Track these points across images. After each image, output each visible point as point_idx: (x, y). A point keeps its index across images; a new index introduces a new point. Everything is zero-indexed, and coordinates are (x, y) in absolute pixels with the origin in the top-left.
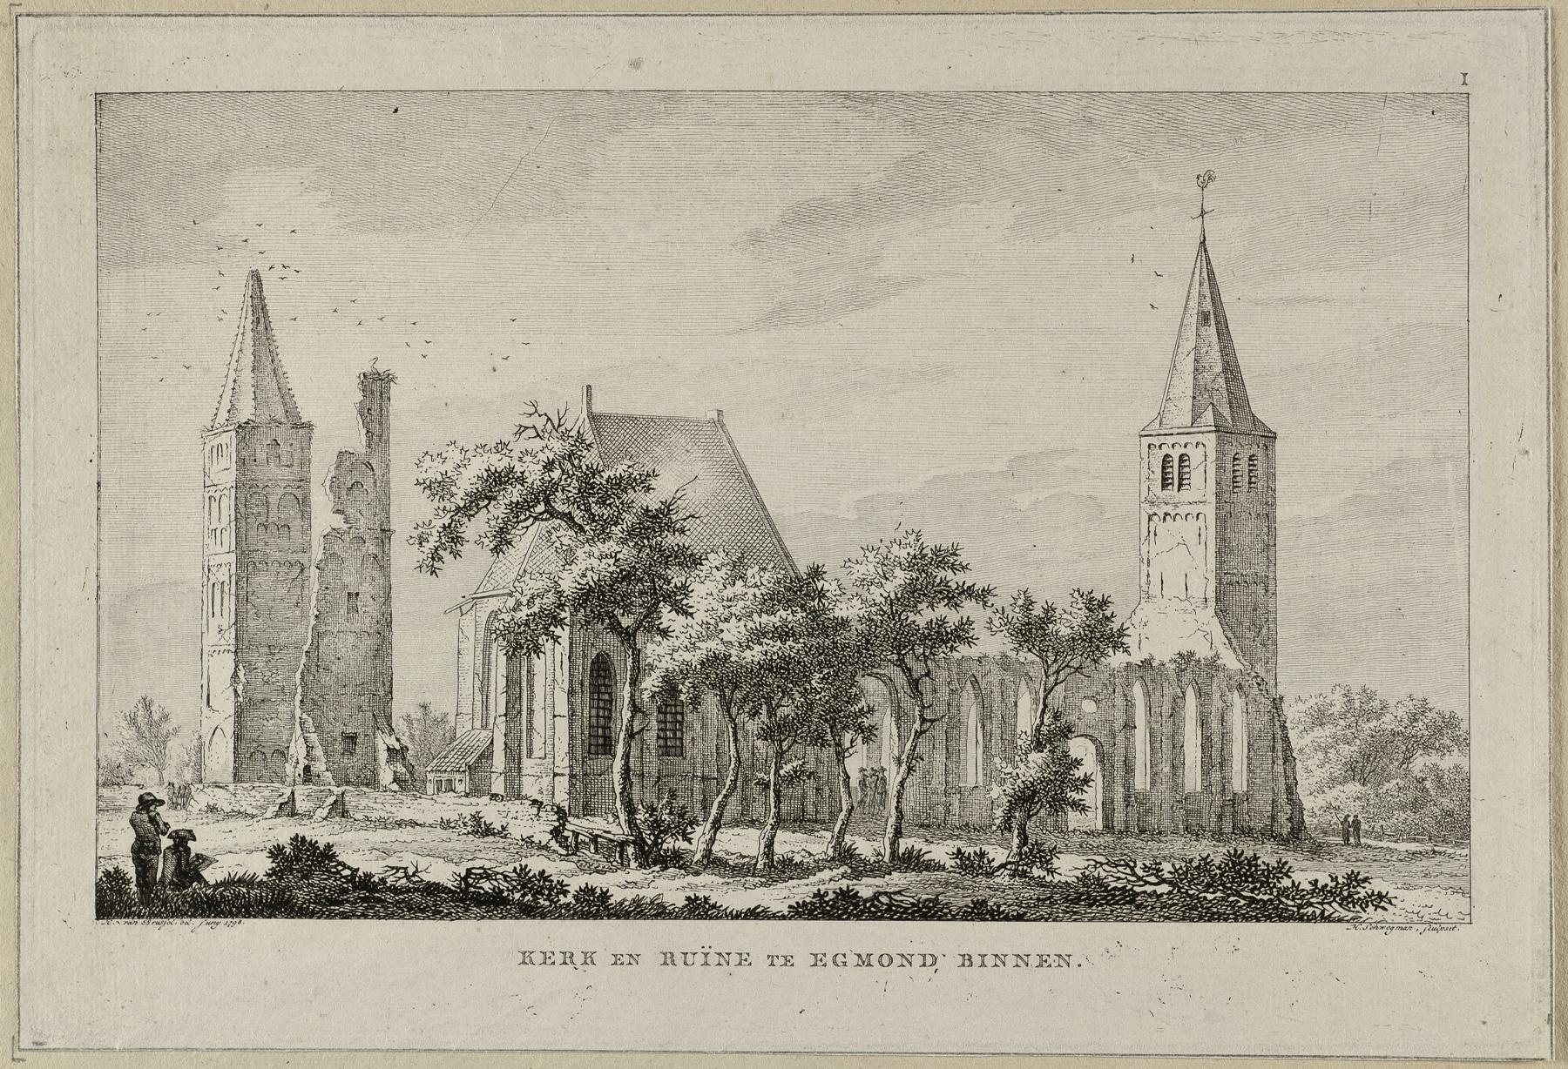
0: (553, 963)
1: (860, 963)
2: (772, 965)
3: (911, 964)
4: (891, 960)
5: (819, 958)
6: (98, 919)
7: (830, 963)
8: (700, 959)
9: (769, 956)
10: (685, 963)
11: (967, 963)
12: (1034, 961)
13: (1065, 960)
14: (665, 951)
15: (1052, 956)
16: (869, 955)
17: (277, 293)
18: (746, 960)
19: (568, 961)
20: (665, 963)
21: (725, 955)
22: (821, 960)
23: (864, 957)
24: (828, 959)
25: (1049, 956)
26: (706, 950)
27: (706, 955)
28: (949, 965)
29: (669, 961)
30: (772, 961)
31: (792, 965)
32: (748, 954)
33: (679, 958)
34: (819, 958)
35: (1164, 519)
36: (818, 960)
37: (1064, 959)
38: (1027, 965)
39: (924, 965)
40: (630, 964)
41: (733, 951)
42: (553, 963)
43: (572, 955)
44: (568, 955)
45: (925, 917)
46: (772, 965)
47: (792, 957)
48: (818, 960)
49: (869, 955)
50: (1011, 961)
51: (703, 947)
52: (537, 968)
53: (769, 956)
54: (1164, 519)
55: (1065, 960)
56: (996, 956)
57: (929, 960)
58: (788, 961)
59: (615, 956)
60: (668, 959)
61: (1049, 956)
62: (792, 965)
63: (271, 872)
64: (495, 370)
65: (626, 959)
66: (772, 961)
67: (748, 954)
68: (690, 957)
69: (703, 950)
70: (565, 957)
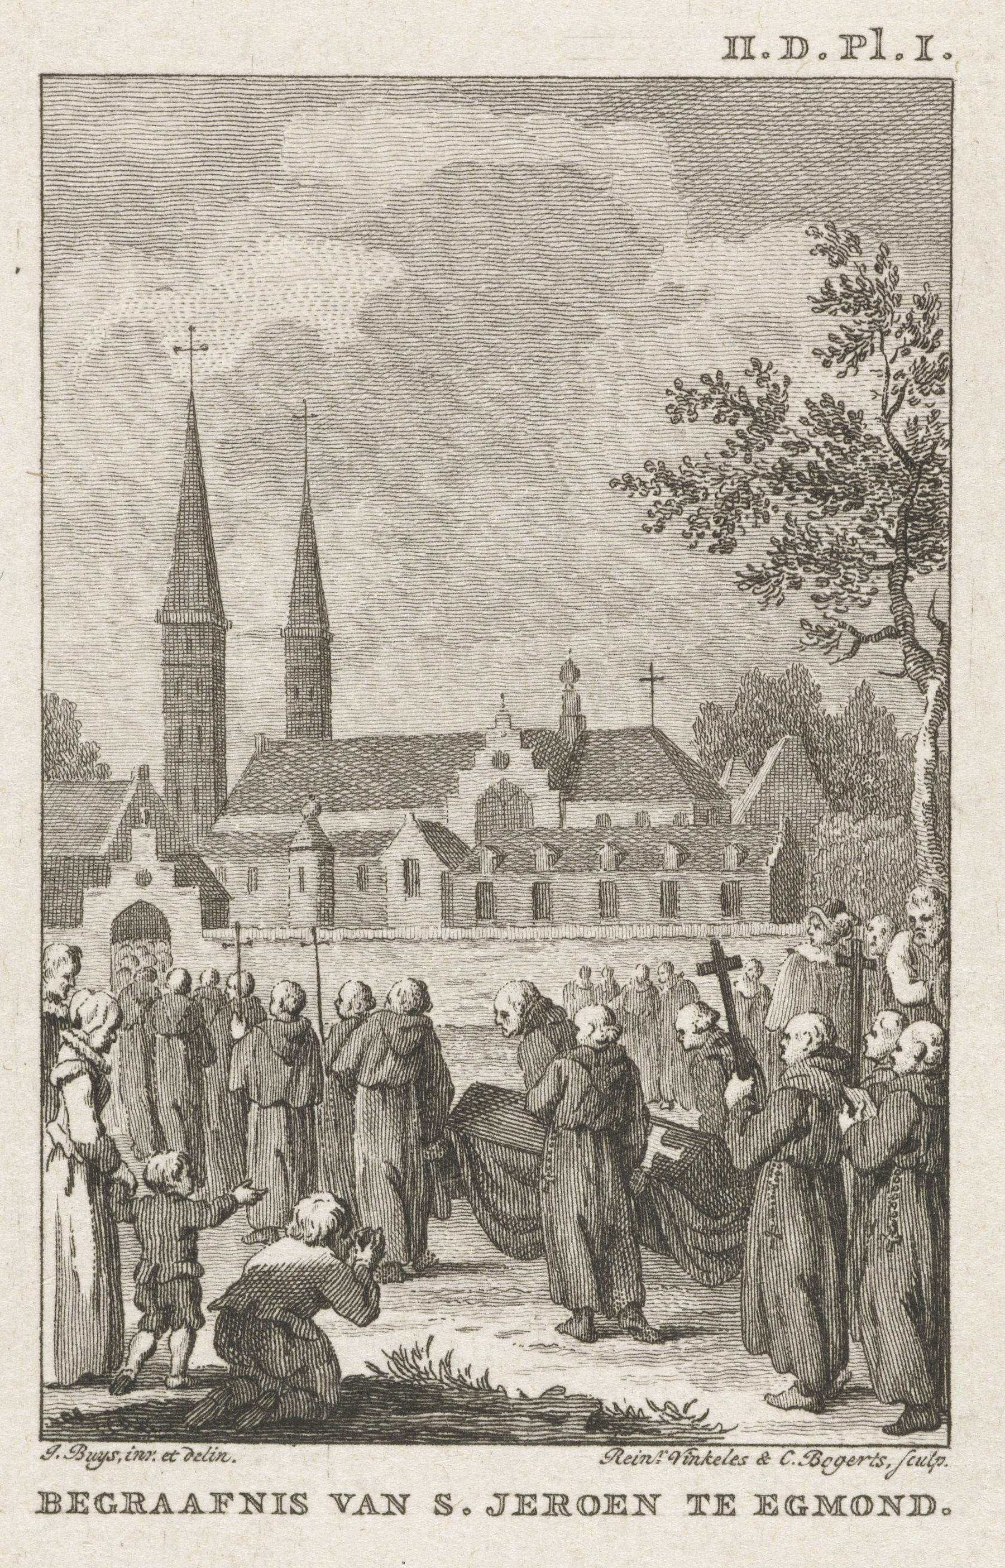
1: (824, 1510)
5: (616, 1502)
6: (114, 941)
7: (92, 1509)
9: (690, 1497)
13: (255, 1502)
15: (539, 1498)
16: (840, 1498)
18: (529, 1505)
21: (649, 1498)
22: (529, 1505)
28: (320, 1505)
31: (733, 1513)
36: (765, 1506)
38: (898, 1513)
44: (559, 1500)
48: (765, 1506)
55: (255, 1502)
62: (733, 1513)
63: (599, 1046)
64: (950, 56)
65: (632, 1504)
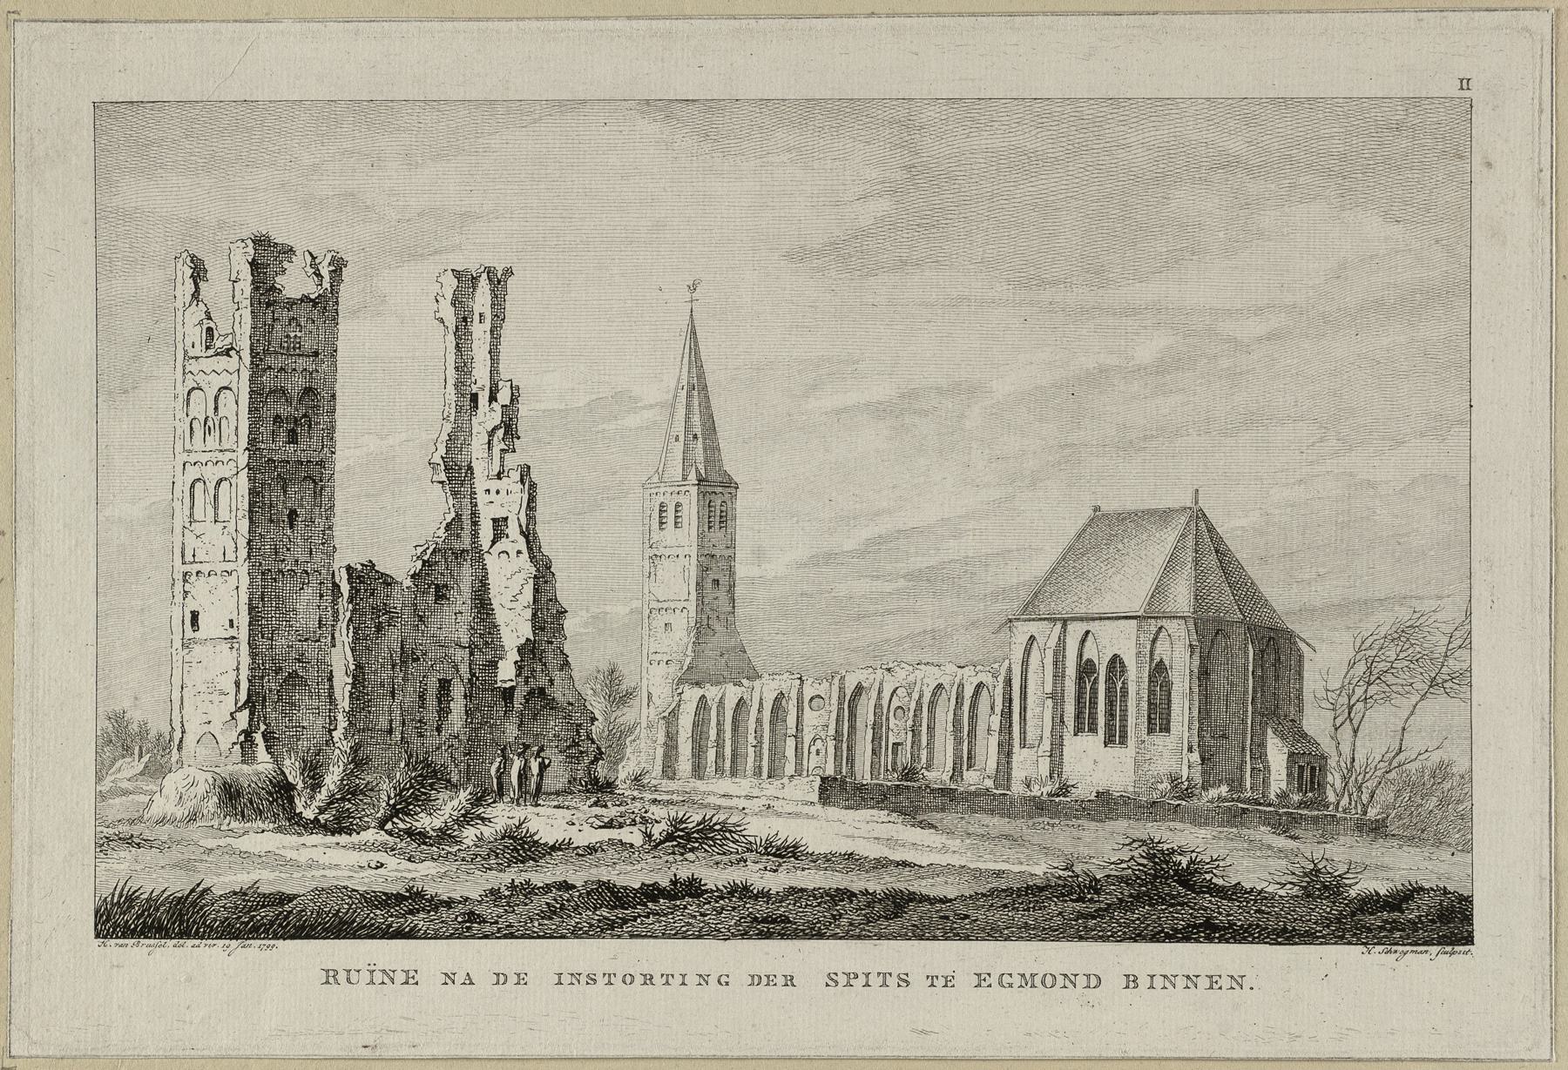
0: (775, 985)
1: (1024, 984)
2: (932, 985)
3: (579, 981)
4: (1043, 983)
5: (411, 975)
8: (366, 976)
10: (348, 980)
11: (1132, 984)
14: (645, 973)
16: (1033, 976)
17: (623, 328)
18: (413, 978)
19: (789, 983)
20: (645, 983)
23: (1028, 977)
24: (994, 980)
25: (1220, 976)
26: (372, 968)
29: (331, 980)
30: (933, 982)
32: (416, 971)
33: (342, 977)
34: (411, 975)
35: (682, 611)
36: (981, 980)
37: (1238, 981)
40: (383, 983)
41: (1203, 974)
42: (1220, 988)
43: (792, 978)
44: (648, 977)
45: (338, 935)
46: (932, 985)
47: (526, 974)
49: (1033, 976)
50: (1181, 982)
51: (369, 965)
52: (779, 988)
53: (928, 977)
54: (682, 611)
56: (572, 974)
57: (502, 978)
58: (948, 982)
59: (979, 975)
60: (500, 978)
61: (1220, 976)
66: (933, 982)
67: (416, 971)
69: (369, 968)
70: (328, 977)
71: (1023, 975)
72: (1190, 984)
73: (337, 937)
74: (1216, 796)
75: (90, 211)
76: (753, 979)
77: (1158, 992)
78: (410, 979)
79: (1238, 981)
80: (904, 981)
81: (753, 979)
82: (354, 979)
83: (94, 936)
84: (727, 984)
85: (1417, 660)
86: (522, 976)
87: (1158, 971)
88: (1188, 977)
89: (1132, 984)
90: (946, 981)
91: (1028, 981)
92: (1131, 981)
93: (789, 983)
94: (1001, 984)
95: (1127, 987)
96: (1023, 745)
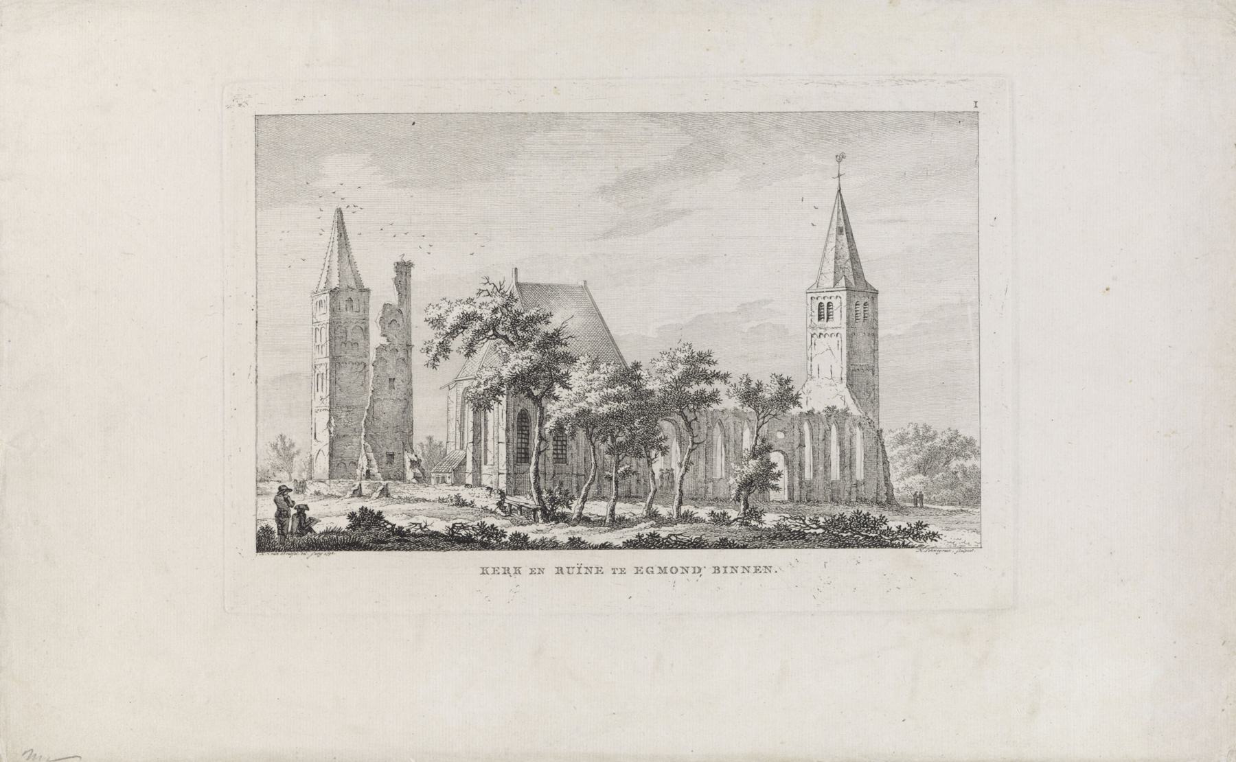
2: (614, 573)
3: (770, 571)
4: (677, 570)
10: (569, 573)
12: (752, 570)
16: (665, 568)
19: (560, 572)
20: (558, 573)
23: (663, 568)
24: (644, 570)
27: (579, 568)
33: (722, 570)
37: (768, 569)
39: (694, 572)
46: (614, 573)
49: (665, 568)
52: (501, 575)
68: (571, 570)
71: (660, 568)
72: (767, 571)
73: (364, 550)
74: (865, 512)
75: (328, 110)
76: (695, 570)
77: (728, 575)
78: (599, 570)
79: (768, 569)
80: (623, 571)
81: (487, 572)
82: (571, 572)
83: (255, 551)
84: (652, 572)
85: (693, 443)
86: (496, 569)
87: (729, 565)
88: (586, 568)
89: (717, 571)
90: (598, 571)
91: (663, 571)
92: (560, 570)
93: (506, 572)
94: (647, 572)
95: (715, 572)
96: (485, 464)
